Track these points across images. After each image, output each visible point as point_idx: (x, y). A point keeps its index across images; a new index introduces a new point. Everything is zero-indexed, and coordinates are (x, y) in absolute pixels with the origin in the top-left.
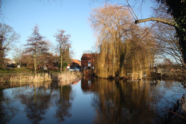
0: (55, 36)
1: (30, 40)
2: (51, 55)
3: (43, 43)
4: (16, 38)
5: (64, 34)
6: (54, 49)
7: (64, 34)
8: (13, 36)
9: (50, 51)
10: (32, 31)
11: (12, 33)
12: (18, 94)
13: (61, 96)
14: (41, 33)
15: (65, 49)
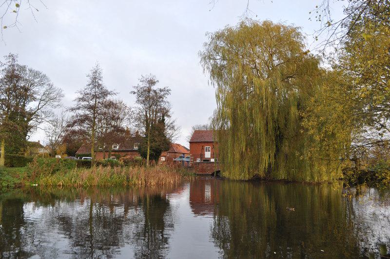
0: (134, 93)
1: (83, 99)
2: (128, 132)
3: (110, 105)
4: (53, 99)
5: (154, 88)
6: (132, 120)
7: (154, 88)
8: (47, 94)
9: (124, 125)
10: (88, 80)
11: (45, 87)
12: (56, 214)
13: (146, 222)
14: (107, 83)
15: (155, 120)
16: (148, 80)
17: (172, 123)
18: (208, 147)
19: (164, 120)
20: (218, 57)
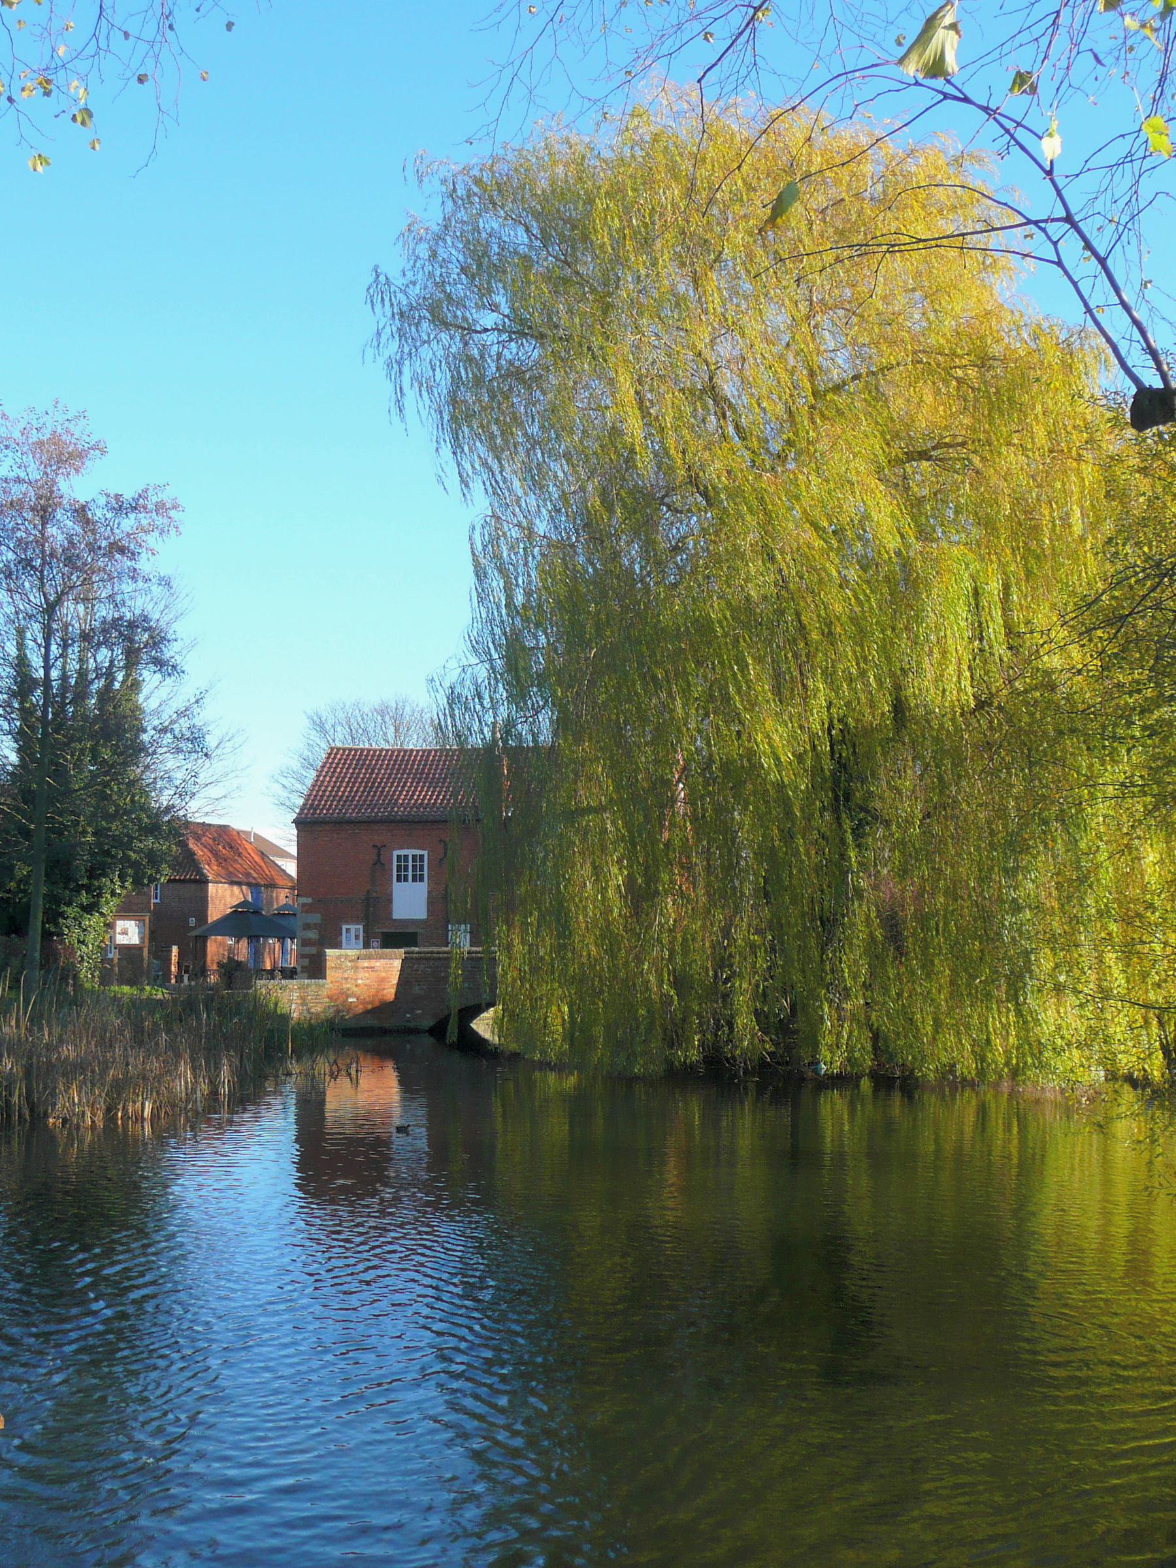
16: (34, 437)
17: (181, 714)
18: (410, 852)
19: (136, 686)
20: (489, 319)
